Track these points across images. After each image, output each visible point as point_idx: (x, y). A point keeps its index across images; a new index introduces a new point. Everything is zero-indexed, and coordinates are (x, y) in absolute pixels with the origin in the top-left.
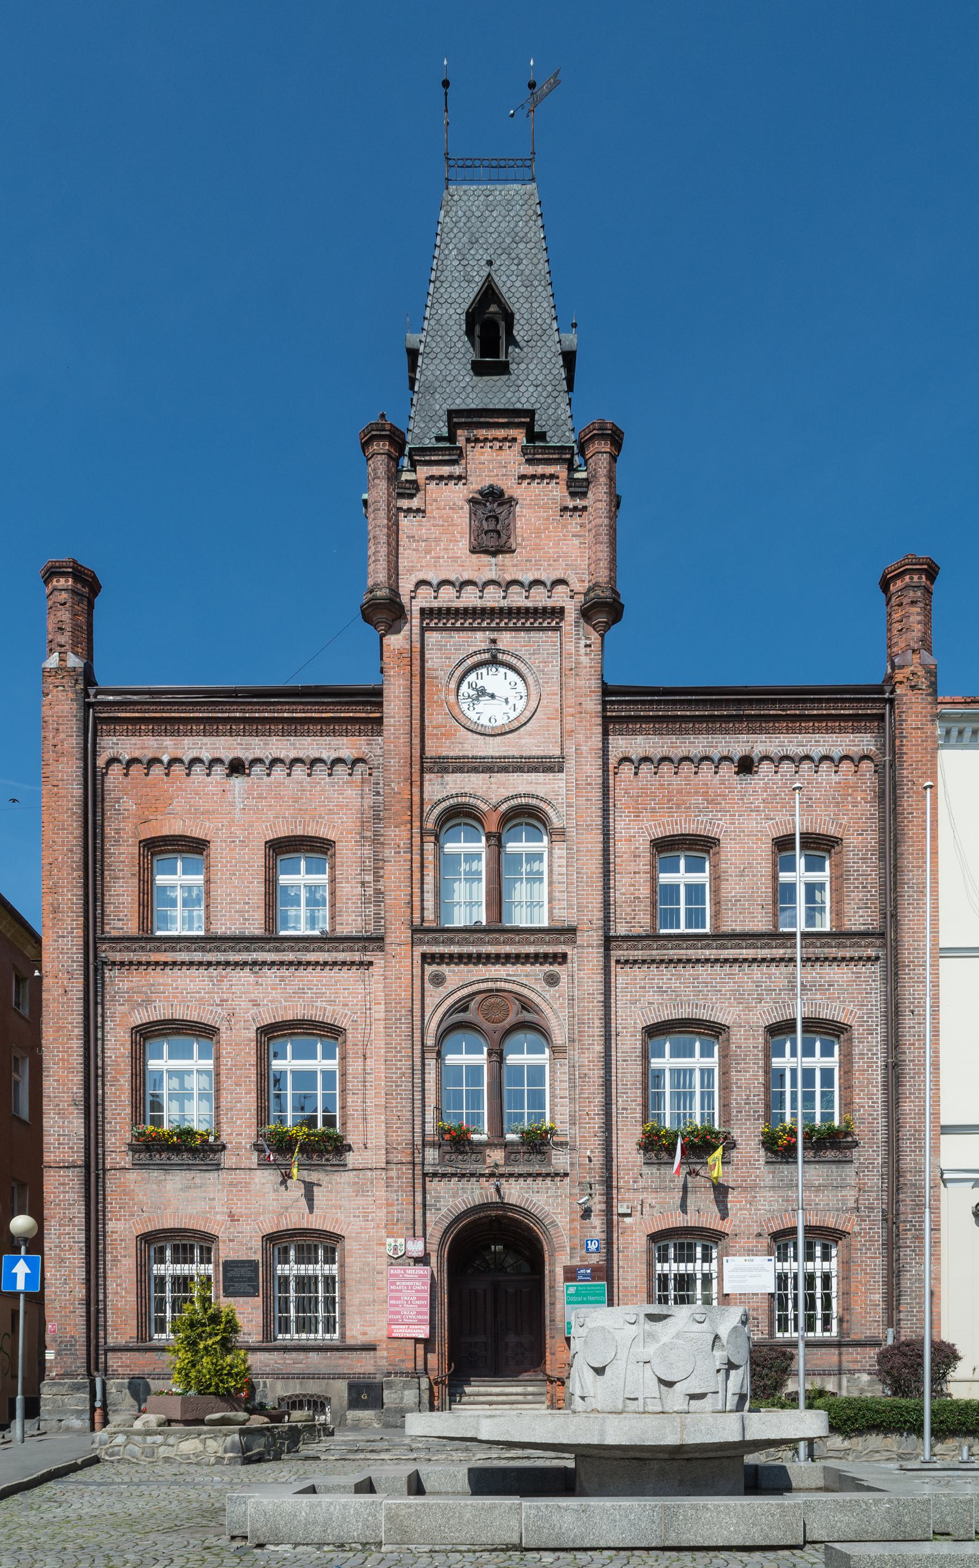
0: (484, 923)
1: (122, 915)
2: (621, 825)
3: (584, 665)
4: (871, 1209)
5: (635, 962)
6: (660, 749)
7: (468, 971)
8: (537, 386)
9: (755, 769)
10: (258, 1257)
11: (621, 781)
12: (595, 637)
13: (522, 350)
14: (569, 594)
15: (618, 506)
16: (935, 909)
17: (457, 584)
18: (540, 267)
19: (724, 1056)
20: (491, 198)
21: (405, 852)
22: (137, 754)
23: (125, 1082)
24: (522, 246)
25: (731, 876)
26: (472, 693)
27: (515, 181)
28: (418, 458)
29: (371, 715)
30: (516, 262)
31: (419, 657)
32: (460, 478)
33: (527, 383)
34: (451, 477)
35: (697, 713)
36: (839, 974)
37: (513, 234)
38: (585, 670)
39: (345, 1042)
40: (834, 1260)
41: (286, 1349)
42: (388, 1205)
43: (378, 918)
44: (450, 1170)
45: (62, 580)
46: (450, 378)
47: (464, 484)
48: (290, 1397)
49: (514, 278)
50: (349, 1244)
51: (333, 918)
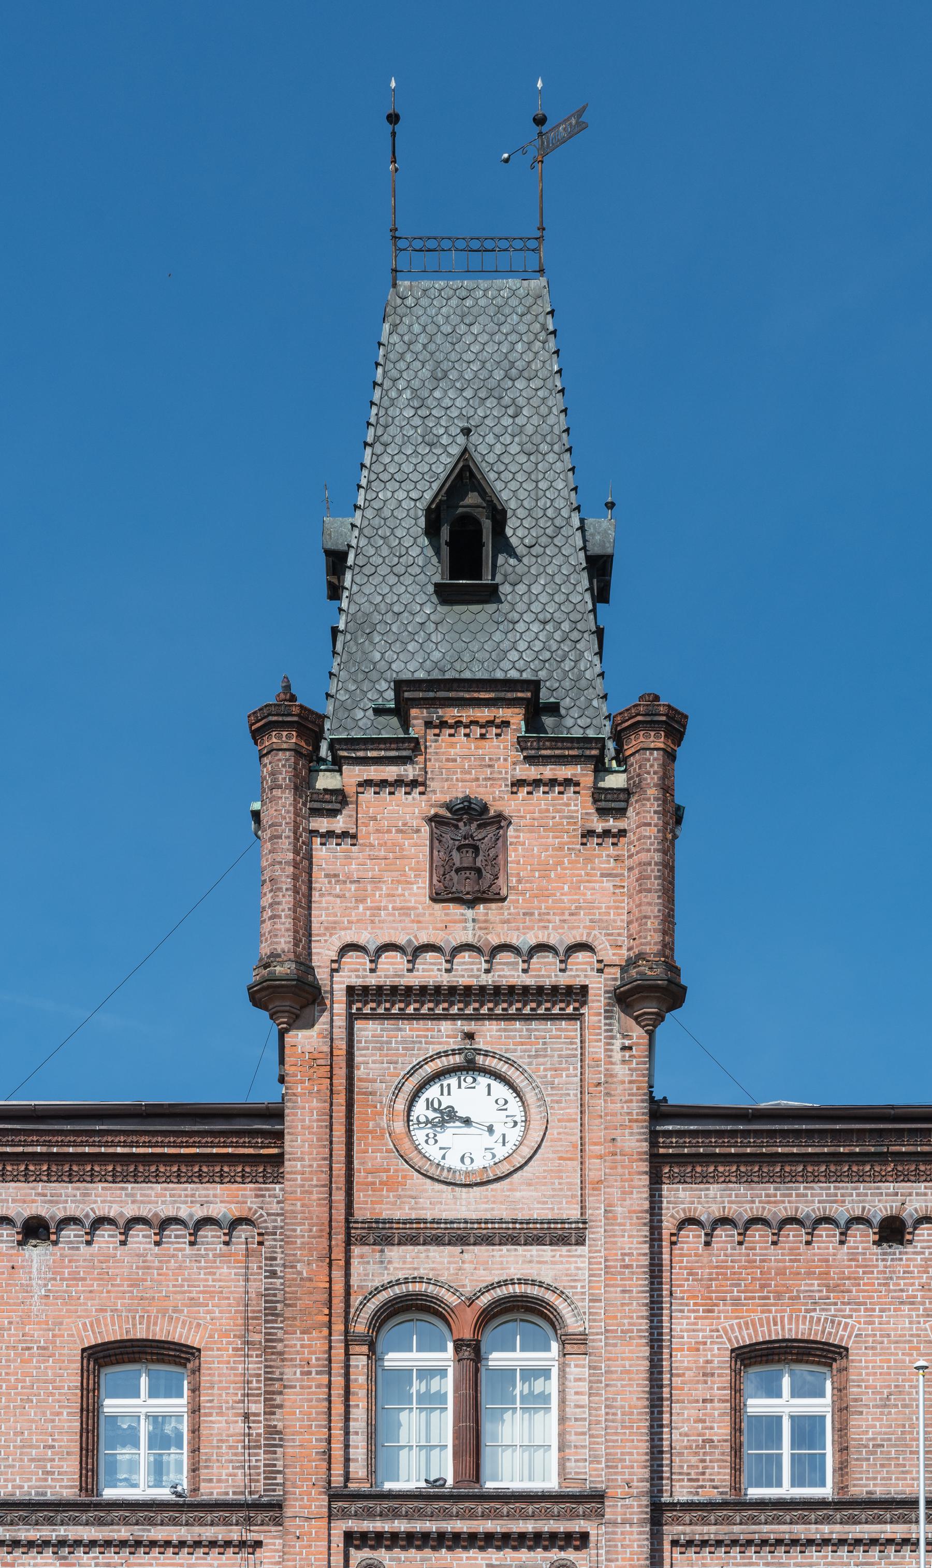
0: (450, 1482)
2: (683, 1325)
3: (620, 1078)
5: (704, 1543)
6: (748, 1206)
7: (423, 1560)
8: (545, 623)
9: (908, 1237)
11: (682, 1255)
12: (638, 1034)
13: (520, 561)
14: (596, 966)
15: (679, 821)
17: (409, 950)
18: (551, 420)
20: (469, 302)
21: (318, 1373)
24: (520, 384)
25: (867, 1406)
26: (431, 1115)
27: (511, 272)
28: (345, 754)
29: (262, 1151)
30: (511, 411)
31: (344, 1064)
33: (528, 617)
34: (400, 782)
35: (810, 1150)
37: (506, 365)
38: (620, 1087)
43: (271, 1472)
46: (403, 621)
47: (421, 793)
49: (507, 439)
51: (194, 1469)
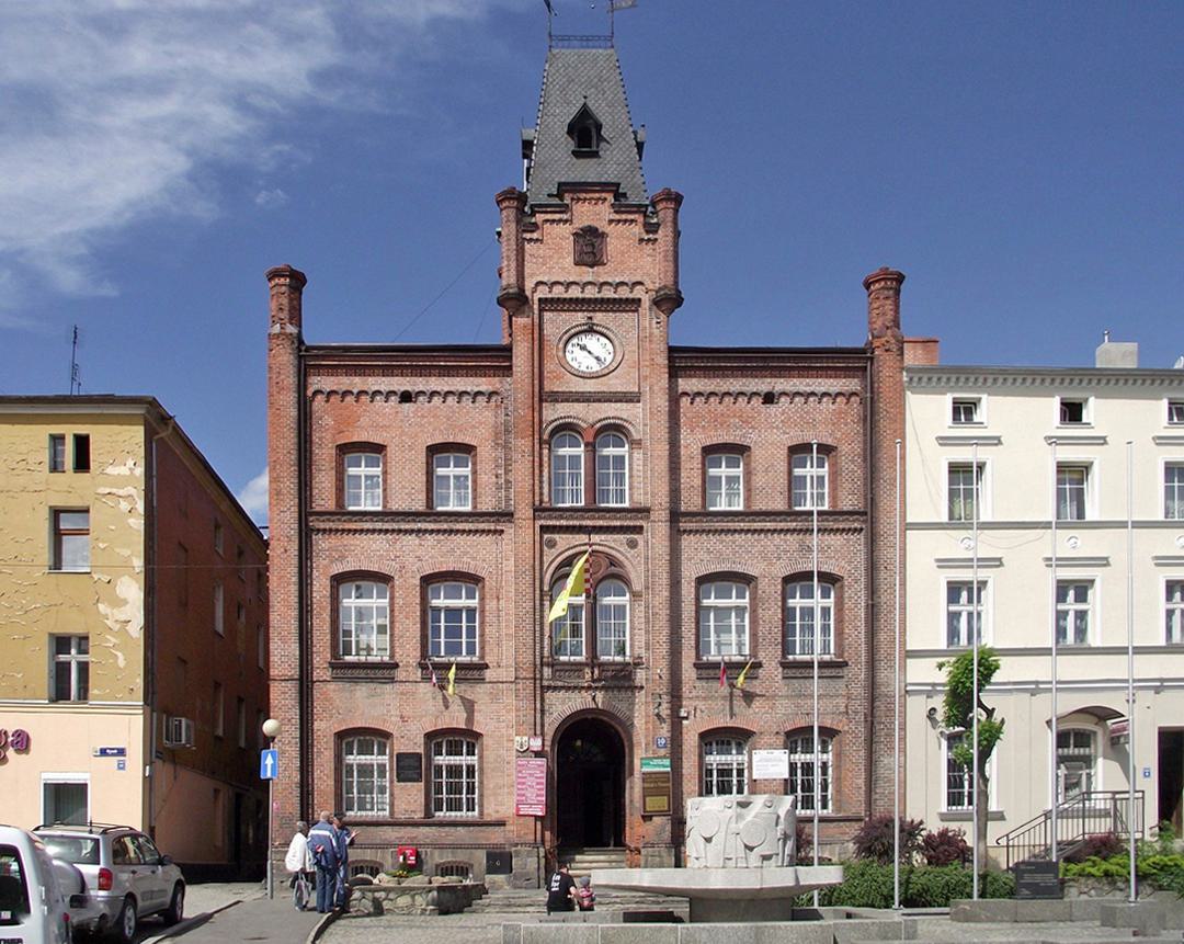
1: (324, 498)
2: (685, 437)
4: (856, 713)
10: (421, 750)
16: (903, 495)
19: (753, 599)
22: (335, 388)
23: (326, 616)
32: (566, 221)
34: (560, 221)
36: (836, 540)
39: (484, 587)
40: (830, 754)
41: (441, 824)
42: (517, 710)
43: (508, 499)
44: (560, 684)
45: (282, 280)
46: (558, 161)
48: (444, 863)
50: (486, 740)
